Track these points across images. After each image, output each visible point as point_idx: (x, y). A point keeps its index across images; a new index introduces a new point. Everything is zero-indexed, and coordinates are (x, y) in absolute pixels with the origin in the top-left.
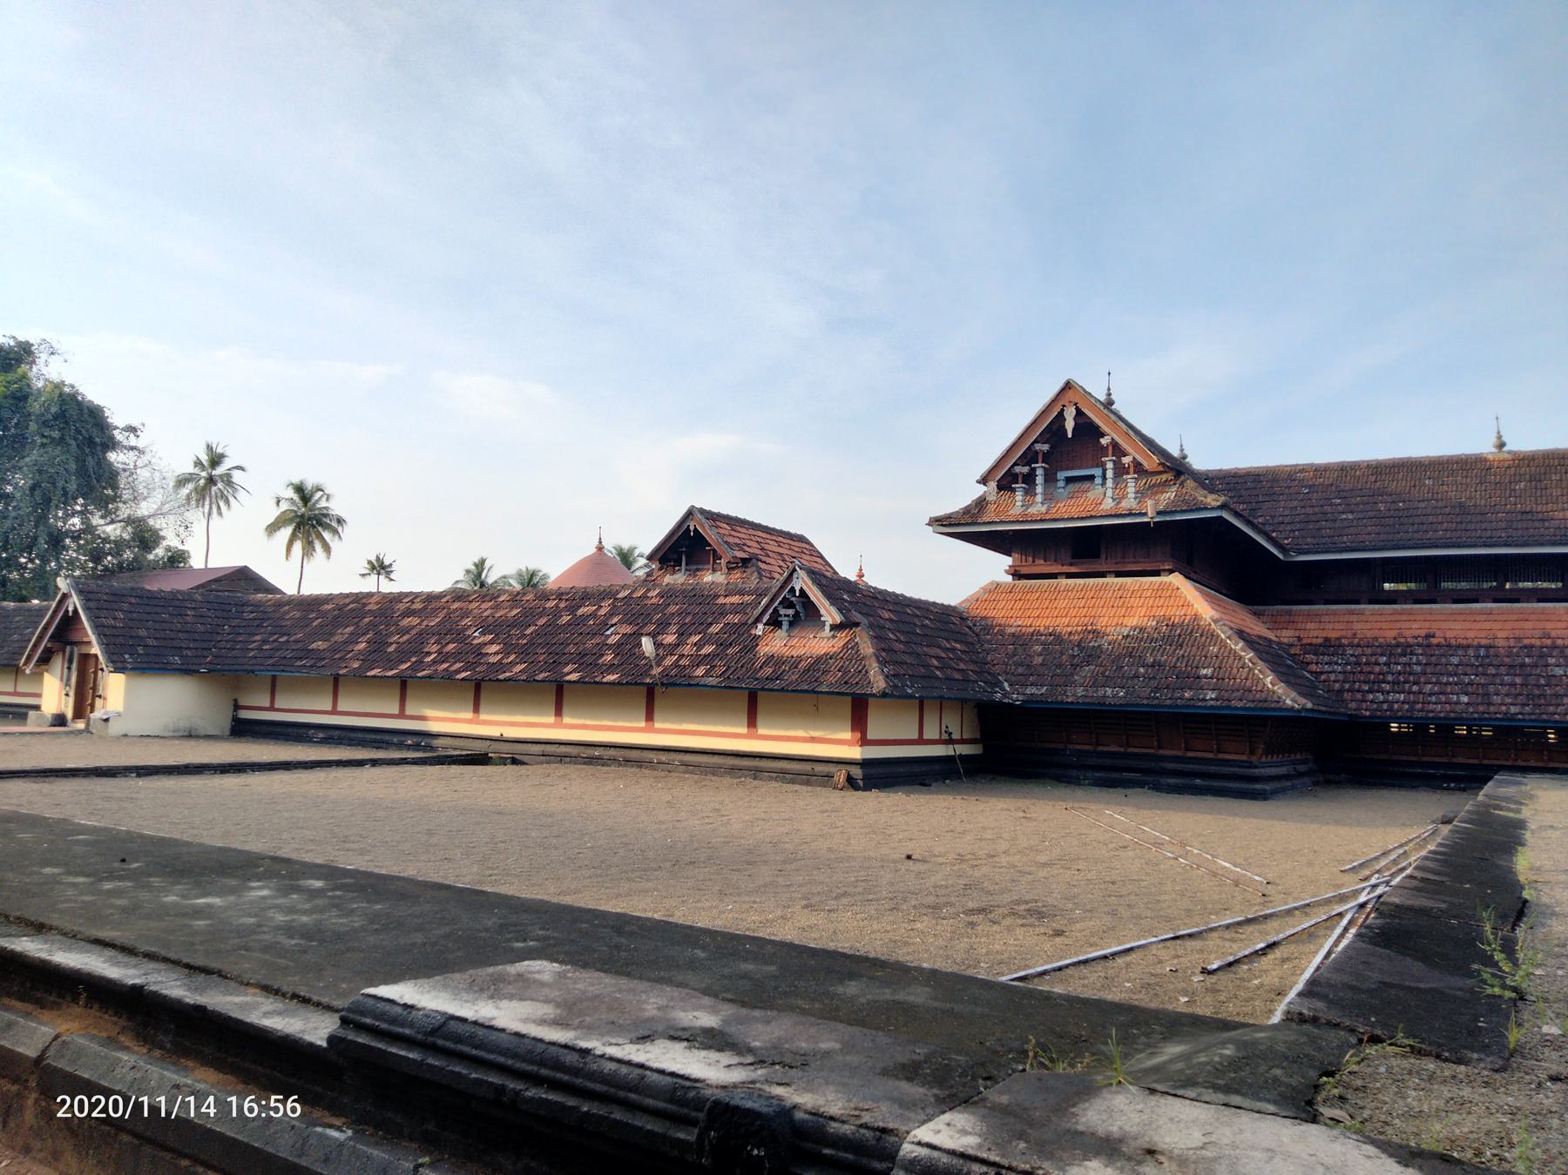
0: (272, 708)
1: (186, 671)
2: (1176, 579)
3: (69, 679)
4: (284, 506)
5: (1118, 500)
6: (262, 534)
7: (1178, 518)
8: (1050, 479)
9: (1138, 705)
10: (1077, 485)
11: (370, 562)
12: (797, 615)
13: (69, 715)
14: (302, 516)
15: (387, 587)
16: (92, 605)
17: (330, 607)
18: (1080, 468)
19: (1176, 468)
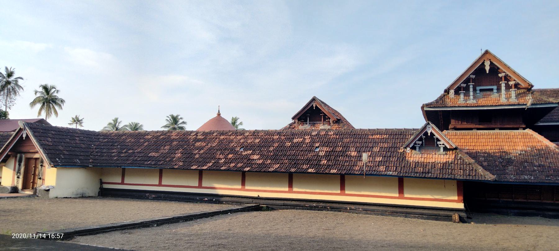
0: (122, 183)
1: (83, 166)
2: (529, 131)
3: (19, 172)
4: (38, 95)
5: (508, 98)
6: (29, 107)
7: (538, 106)
8: (475, 90)
9: (544, 183)
10: (485, 93)
11: (73, 119)
12: (422, 144)
13: (20, 187)
14: (47, 99)
15: (79, 127)
16: (36, 134)
17: (150, 137)
18: (483, 86)
19: (529, 89)
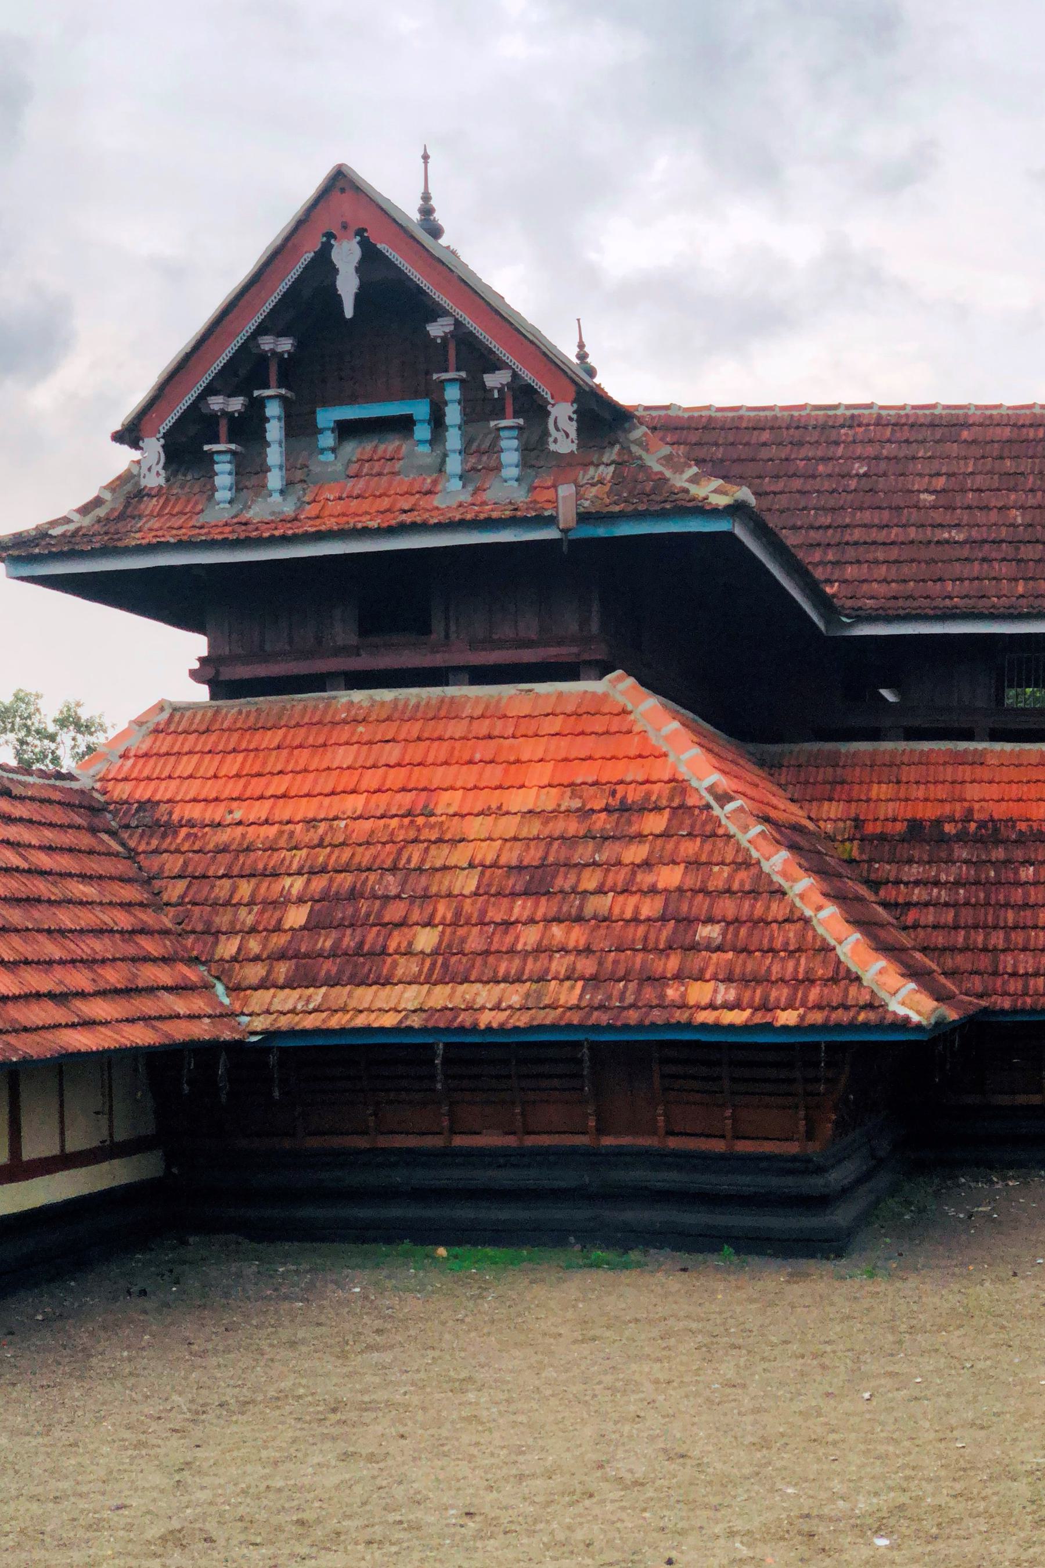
8: (300, 427)
18: (353, 399)
